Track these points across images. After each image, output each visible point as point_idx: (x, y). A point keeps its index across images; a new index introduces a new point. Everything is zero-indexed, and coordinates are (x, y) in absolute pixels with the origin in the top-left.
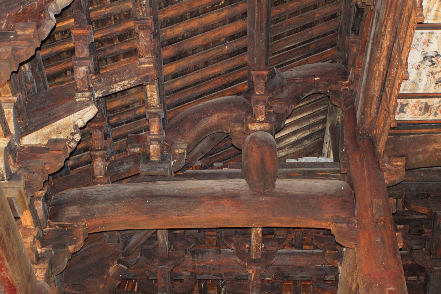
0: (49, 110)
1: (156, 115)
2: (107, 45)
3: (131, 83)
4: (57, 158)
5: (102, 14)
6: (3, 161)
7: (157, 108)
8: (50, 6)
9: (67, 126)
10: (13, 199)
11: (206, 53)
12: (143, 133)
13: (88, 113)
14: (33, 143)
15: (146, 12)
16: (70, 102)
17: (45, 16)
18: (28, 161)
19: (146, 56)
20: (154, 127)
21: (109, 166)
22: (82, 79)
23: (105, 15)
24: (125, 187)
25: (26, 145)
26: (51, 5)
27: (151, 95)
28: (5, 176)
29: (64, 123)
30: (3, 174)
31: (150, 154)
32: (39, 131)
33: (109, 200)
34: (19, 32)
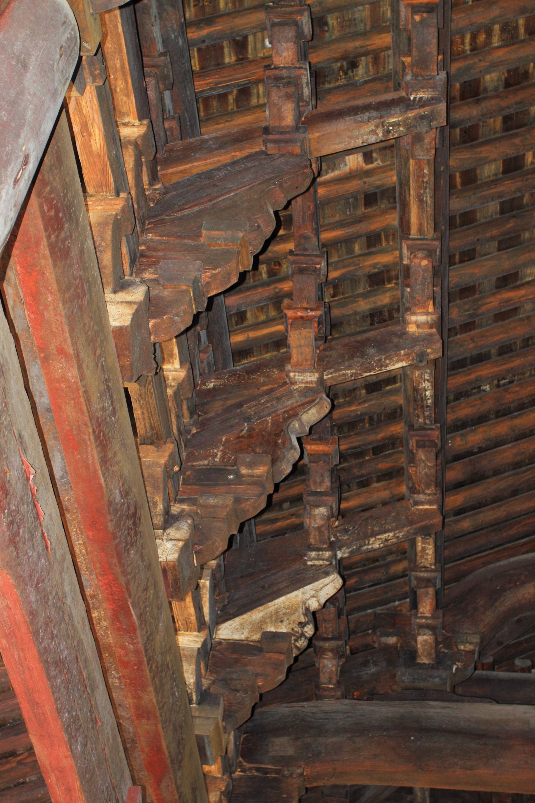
0: (262, 579)
1: (428, 582)
2: (353, 462)
3: (398, 537)
4: (276, 666)
5: (353, 415)
6: (194, 673)
7: (432, 571)
8: (291, 426)
9: (291, 610)
10: (205, 738)
11: (517, 474)
12: (397, 603)
13: (326, 588)
14: (236, 637)
15: (429, 417)
16: (297, 566)
17: (284, 443)
18: (228, 670)
19: (426, 491)
20: (424, 604)
21: (343, 666)
22: (319, 529)
23: (357, 416)
24: (372, 708)
25: (225, 640)
26: (293, 423)
27: (424, 549)
28: (194, 697)
29: (288, 603)
30: (191, 693)
31: (416, 651)
32: (245, 616)
33: (345, 730)
34: (244, 471)
